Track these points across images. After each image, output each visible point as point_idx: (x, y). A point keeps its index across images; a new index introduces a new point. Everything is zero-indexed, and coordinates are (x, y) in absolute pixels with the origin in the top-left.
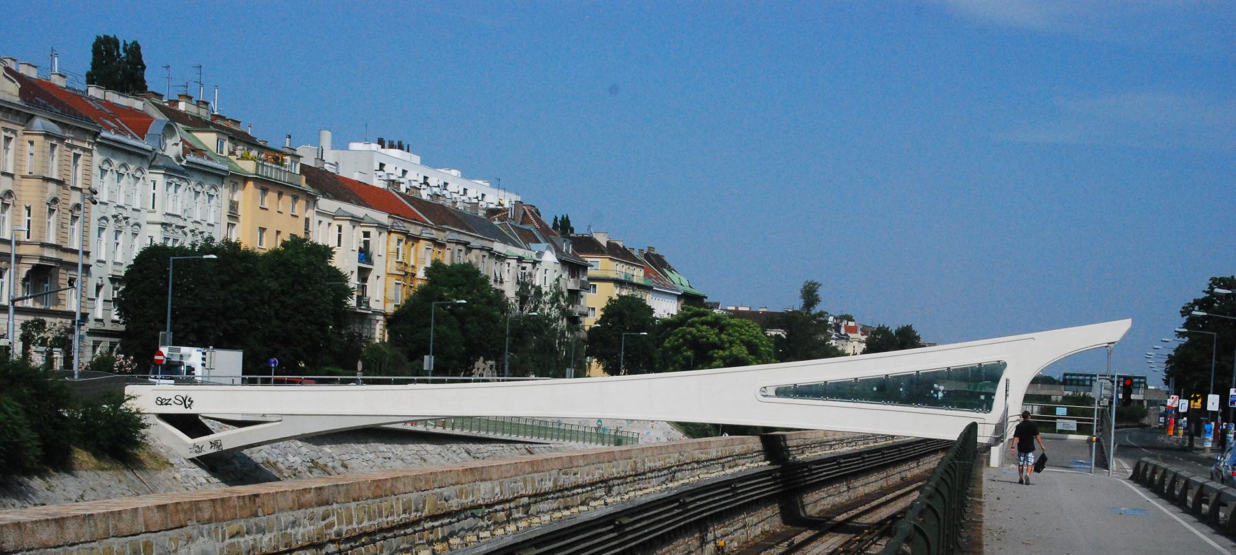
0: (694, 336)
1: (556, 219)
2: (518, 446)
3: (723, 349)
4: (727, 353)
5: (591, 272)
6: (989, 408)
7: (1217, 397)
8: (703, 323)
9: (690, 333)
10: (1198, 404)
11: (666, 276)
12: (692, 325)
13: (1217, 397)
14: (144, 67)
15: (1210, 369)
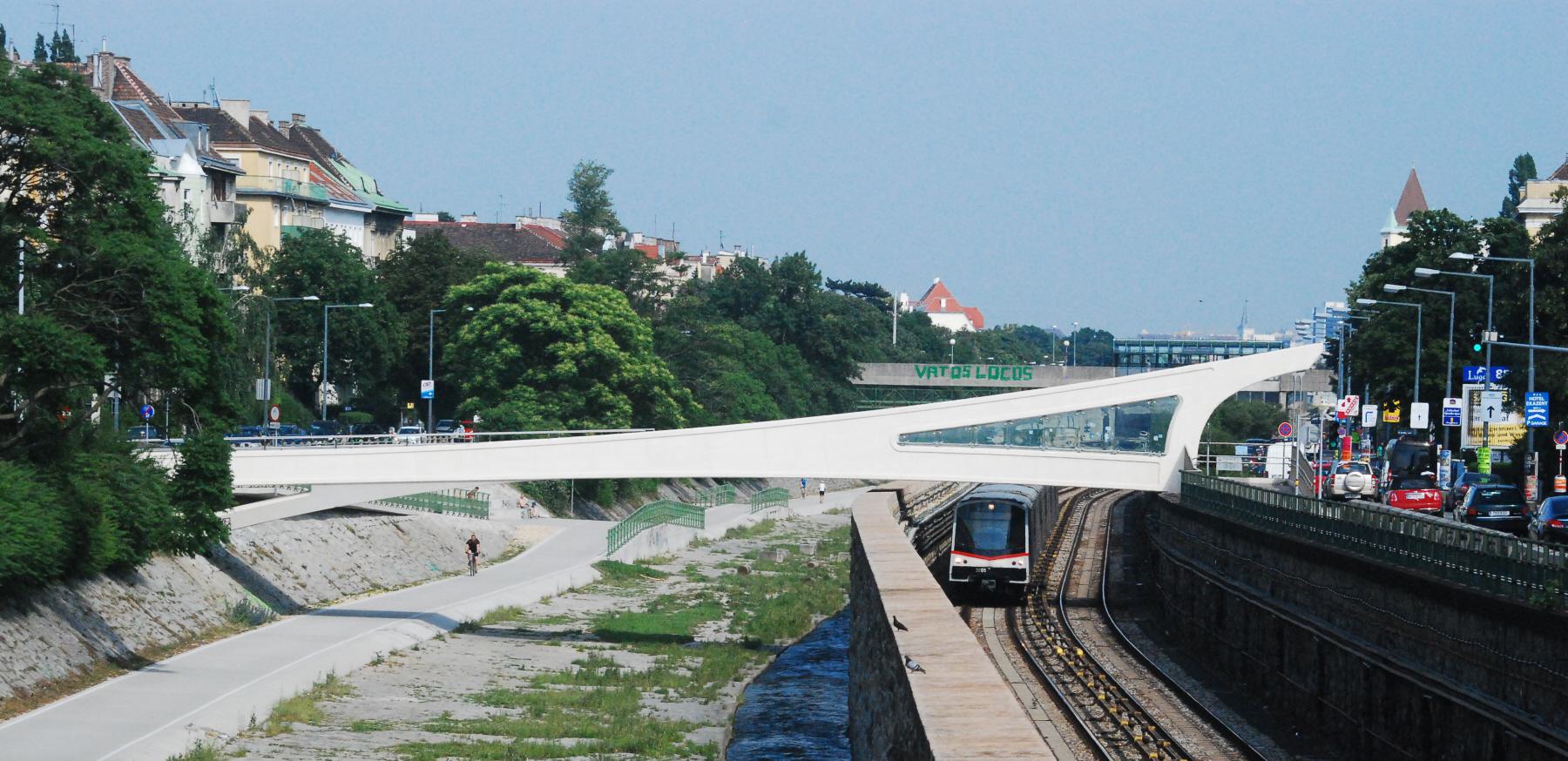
0: (519, 319)
1: (40, 40)
2: (384, 518)
3: (573, 342)
4: (582, 347)
5: (241, 183)
6: (1158, 447)
7: (1425, 406)
8: (532, 295)
9: (512, 314)
10: (1394, 416)
11: (338, 176)
12: (513, 299)
13: (1425, 406)
14: (795, 271)
15: (1413, 362)
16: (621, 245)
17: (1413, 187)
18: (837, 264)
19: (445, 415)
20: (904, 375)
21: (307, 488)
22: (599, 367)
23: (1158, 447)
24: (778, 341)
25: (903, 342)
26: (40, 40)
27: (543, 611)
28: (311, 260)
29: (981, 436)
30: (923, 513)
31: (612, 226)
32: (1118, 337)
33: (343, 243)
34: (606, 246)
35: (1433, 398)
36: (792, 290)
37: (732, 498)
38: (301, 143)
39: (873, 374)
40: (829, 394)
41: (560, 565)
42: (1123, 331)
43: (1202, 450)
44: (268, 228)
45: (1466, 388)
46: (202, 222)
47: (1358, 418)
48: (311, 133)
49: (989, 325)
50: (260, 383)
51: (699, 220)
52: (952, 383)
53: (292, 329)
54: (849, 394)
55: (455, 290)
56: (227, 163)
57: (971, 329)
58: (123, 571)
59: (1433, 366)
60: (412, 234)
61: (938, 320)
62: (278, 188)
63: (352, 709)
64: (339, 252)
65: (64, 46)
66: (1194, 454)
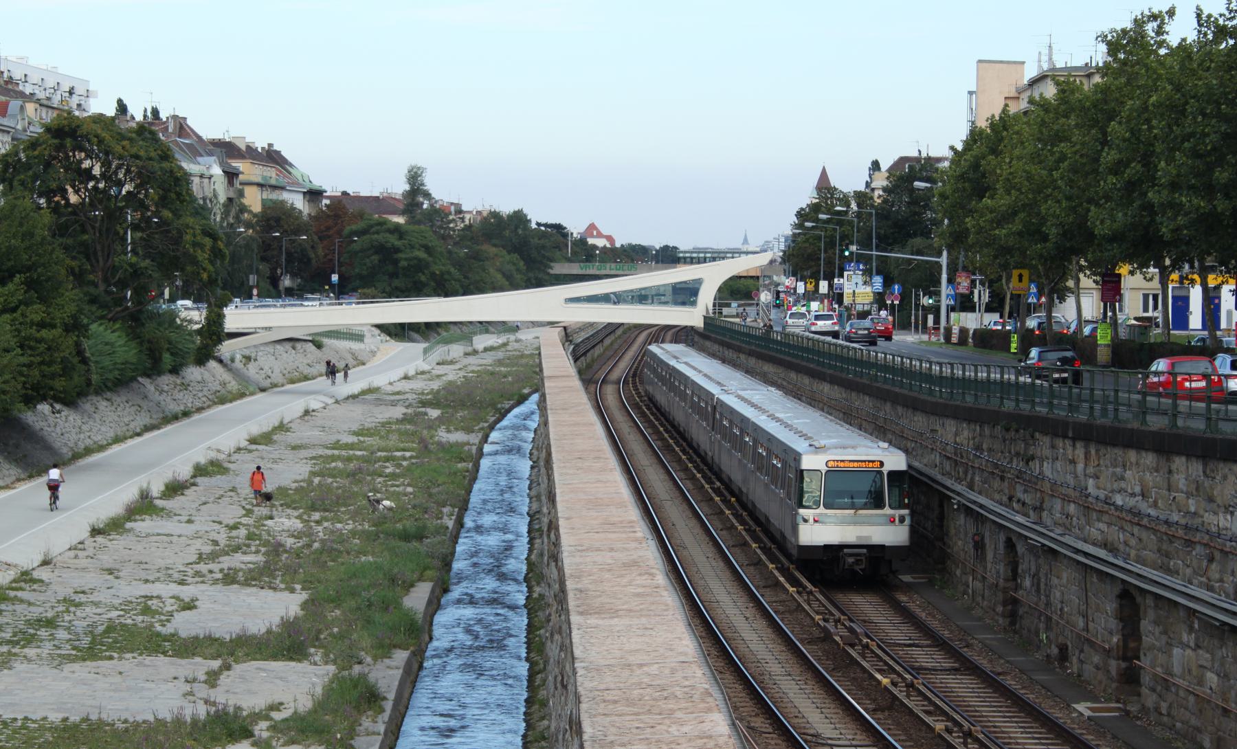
1: (145, 110)
6: (694, 304)
12: (377, 233)
16: (432, 205)
17: (824, 175)
18: (538, 215)
19: (342, 291)
20: (575, 269)
21: (269, 329)
22: (419, 266)
23: (694, 304)
24: (509, 252)
25: (574, 253)
26: (145, 110)
27: (389, 389)
28: (276, 216)
29: (605, 298)
30: (579, 339)
31: (427, 195)
32: (682, 248)
33: (293, 208)
34: (425, 206)
35: (829, 277)
36: (517, 227)
37: (487, 332)
38: (272, 157)
39: (558, 269)
40: (536, 278)
41: (395, 368)
42: (684, 244)
43: (714, 305)
44: (254, 200)
45: (846, 273)
46: (222, 198)
47: (795, 289)
48: (278, 153)
49: (618, 245)
50: (251, 277)
51: (471, 187)
52: (598, 273)
53: (267, 250)
54: (547, 277)
55: (347, 230)
56: (235, 168)
57: (608, 246)
58: (175, 371)
59: (830, 263)
60: (328, 202)
61: (591, 241)
62: (259, 180)
63: (291, 438)
64: (291, 212)
65: (155, 112)
66: (711, 307)
